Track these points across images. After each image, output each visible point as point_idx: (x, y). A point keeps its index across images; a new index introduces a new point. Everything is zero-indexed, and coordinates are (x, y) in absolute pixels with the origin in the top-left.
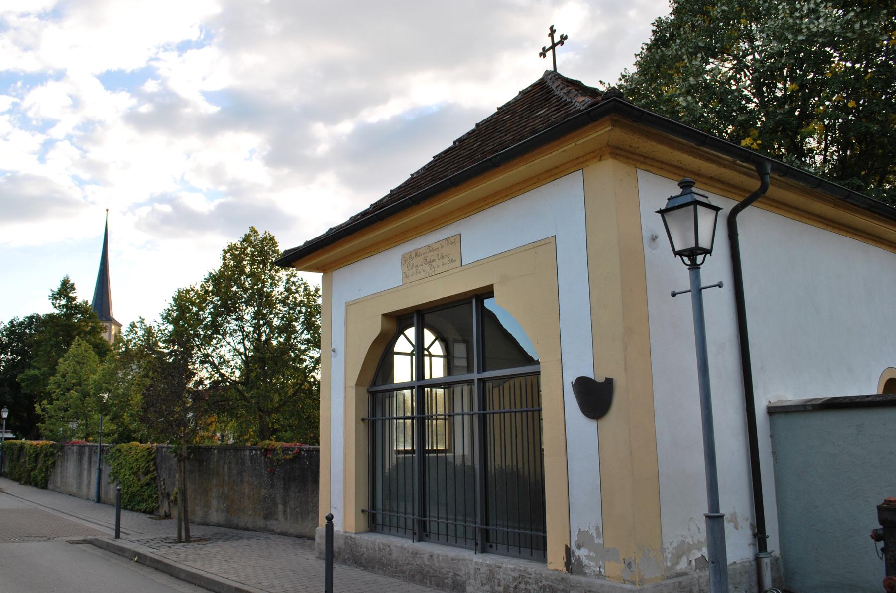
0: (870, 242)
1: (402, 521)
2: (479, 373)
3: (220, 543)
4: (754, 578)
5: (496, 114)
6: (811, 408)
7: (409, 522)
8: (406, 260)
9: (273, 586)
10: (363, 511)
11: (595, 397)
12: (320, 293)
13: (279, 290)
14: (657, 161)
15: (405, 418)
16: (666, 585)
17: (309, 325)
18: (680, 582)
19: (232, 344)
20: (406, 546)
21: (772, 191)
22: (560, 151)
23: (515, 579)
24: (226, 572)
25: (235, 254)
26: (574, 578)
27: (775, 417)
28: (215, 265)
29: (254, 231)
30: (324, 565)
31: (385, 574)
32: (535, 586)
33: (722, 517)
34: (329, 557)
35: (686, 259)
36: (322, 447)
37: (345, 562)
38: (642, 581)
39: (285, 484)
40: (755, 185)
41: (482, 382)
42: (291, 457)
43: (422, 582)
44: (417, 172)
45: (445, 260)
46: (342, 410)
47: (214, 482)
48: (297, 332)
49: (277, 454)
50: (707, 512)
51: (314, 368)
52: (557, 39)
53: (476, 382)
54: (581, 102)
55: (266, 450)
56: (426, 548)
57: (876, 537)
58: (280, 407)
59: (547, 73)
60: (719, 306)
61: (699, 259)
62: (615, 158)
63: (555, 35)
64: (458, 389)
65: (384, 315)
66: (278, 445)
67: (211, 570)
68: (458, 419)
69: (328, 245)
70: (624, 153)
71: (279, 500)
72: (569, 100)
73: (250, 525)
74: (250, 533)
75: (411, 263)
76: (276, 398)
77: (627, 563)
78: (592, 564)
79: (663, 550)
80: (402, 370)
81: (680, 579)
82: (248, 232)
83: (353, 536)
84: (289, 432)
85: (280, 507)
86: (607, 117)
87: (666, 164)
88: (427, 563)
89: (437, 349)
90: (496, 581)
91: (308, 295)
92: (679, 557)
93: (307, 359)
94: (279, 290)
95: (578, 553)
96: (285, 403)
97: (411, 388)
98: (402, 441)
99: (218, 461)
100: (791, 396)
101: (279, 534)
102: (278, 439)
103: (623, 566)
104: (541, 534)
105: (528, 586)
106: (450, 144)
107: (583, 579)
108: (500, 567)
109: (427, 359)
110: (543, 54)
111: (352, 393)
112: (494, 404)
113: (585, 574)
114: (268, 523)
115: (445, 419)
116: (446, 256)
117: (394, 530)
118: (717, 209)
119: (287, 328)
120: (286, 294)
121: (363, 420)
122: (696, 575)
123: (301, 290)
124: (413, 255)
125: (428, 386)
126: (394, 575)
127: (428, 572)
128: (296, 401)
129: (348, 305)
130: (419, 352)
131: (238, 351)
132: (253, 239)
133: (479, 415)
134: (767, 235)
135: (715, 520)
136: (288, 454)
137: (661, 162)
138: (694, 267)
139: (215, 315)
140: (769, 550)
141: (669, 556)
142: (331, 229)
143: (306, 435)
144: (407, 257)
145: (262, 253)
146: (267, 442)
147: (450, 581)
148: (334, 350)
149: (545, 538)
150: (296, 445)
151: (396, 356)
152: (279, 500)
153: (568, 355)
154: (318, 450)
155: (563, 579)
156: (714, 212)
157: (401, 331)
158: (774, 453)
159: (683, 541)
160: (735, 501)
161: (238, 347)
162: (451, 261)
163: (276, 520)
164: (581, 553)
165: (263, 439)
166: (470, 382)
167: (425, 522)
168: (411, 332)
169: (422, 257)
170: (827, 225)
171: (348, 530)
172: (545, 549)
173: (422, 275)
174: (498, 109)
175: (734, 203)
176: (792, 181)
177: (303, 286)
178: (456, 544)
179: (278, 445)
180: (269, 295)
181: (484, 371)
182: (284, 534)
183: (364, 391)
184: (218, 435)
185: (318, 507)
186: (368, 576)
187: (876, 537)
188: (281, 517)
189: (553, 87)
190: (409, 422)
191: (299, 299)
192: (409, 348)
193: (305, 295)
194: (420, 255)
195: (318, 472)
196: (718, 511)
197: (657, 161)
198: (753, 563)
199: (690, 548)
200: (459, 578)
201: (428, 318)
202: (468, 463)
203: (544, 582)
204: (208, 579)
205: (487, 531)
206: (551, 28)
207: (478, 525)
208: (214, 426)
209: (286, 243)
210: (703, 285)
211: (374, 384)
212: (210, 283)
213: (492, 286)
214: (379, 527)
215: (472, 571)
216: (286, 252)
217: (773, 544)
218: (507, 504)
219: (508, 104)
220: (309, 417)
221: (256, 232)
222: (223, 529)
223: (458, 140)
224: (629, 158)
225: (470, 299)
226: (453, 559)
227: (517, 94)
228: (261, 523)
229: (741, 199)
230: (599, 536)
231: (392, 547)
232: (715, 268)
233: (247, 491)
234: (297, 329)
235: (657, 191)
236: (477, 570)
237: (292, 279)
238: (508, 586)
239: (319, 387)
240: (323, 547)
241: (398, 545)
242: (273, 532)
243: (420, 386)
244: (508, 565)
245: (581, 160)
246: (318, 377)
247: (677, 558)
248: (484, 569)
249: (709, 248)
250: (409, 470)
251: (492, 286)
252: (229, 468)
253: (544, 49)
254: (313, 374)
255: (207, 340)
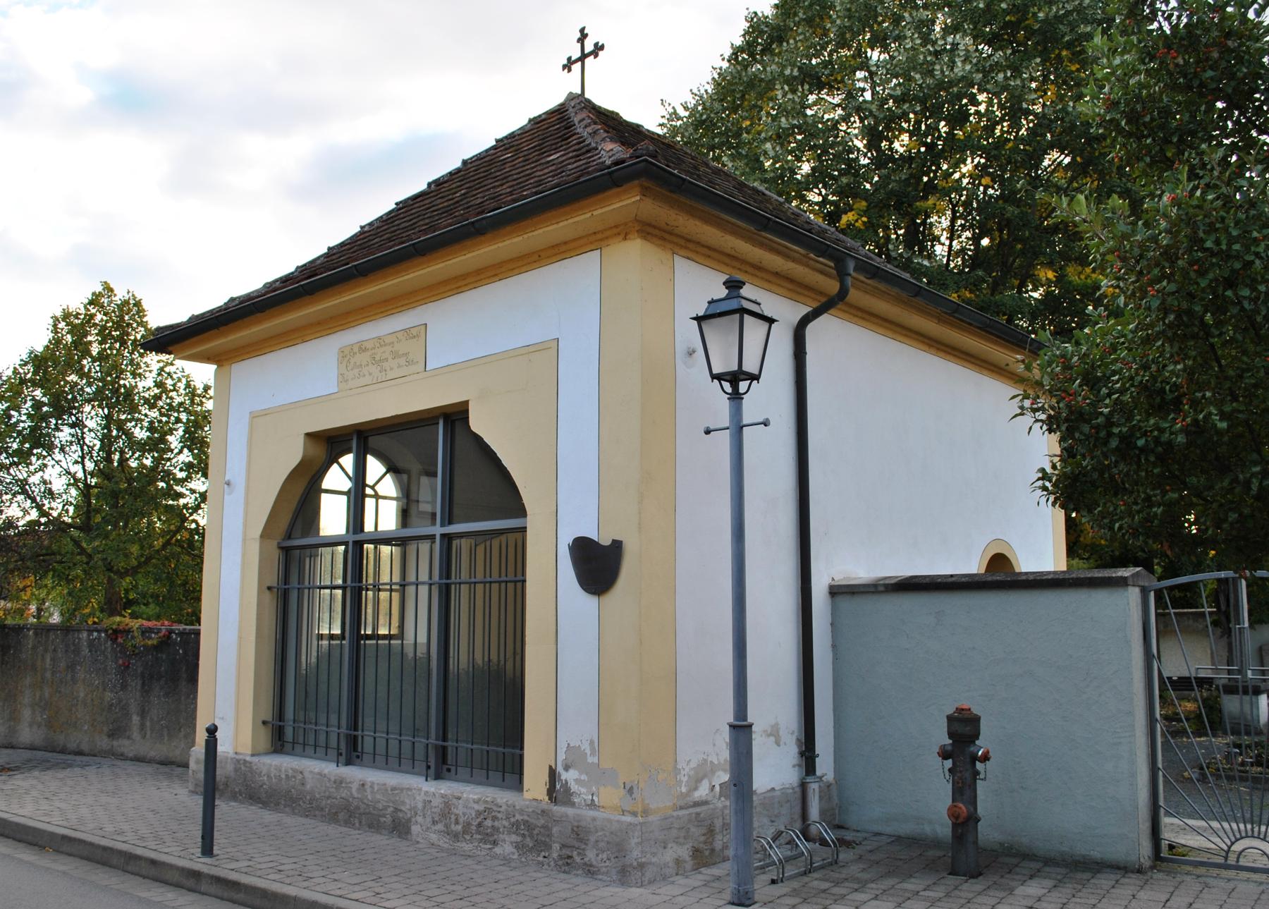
0: (986, 372)
1: (322, 738)
2: (442, 525)
3: (36, 773)
4: (798, 809)
5: (493, 148)
6: (882, 589)
7: (333, 738)
8: (345, 356)
9: (122, 833)
10: (264, 723)
11: (597, 565)
12: (211, 392)
13: (146, 385)
14: (703, 246)
15: (333, 588)
16: (678, 818)
17: (194, 441)
18: (698, 814)
19: (64, 464)
20: (326, 771)
21: (854, 295)
22: (571, 221)
23: (479, 813)
24: (46, 815)
25: (74, 329)
26: (558, 810)
27: (839, 599)
28: (40, 340)
29: (109, 289)
30: (201, 802)
31: (294, 814)
32: (506, 823)
33: (750, 726)
34: (211, 790)
35: (727, 386)
36: (205, 627)
37: (234, 797)
38: (646, 812)
39: (143, 684)
40: (833, 287)
41: (448, 538)
42: (155, 642)
43: (347, 823)
44: (370, 224)
45: (402, 361)
46: (237, 574)
47: (28, 681)
48: (172, 451)
49: (133, 637)
50: (731, 719)
51: (197, 508)
52: (589, 47)
53: (438, 538)
54: (610, 150)
55: (116, 632)
56: (355, 774)
57: (945, 754)
58: (140, 565)
59: (571, 97)
60: (770, 453)
61: (743, 386)
62: (645, 238)
63: (586, 42)
64: (412, 548)
65: (308, 435)
66: (135, 624)
67: (21, 812)
68: (411, 590)
69: (226, 324)
70: (656, 232)
71: (133, 708)
72: (593, 145)
73: (85, 747)
74: (85, 758)
75: (352, 361)
76: (135, 549)
77: (628, 787)
78: (583, 790)
79: (676, 771)
80: (333, 518)
81: (698, 810)
82: (99, 289)
83: (248, 758)
84: (152, 606)
85: (136, 719)
86: (636, 182)
87: (714, 250)
88: (356, 795)
89: (388, 487)
90: (453, 817)
91: (192, 393)
92: (699, 781)
93: (188, 493)
94: (146, 385)
95: (565, 776)
96: (149, 559)
97: (346, 544)
98: (328, 622)
99: (34, 648)
100: (863, 572)
101: (131, 760)
102: (134, 616)
103: (622, 792)
104: (518, 751)
105: (496, 824)
106: (423, 187)
107: (570, 811)
108: (459, 798)
109: (370, 504)
110: (568, 66)
111: (255, 548)
112: (462, 571)
113: (573, 804)
114: (115, 743)
115: (391, 590)
116: (406, 354)
117: (310, 750)
118: (771, 321)
119: (157, 443)
120: (157, 391)
121: (269, 588)
122: (720, 805)
123: (182, 385)
124: (356, 349)
125: (370, 542)
126: (307, 814)
127: (358, 808)
128: (167, 558)
129: (254, 416)
130: (358, 495)
131: (74, 476)
132: (105, 300)
133: (440, 585)
134: (848, 353)
135: (741, 730)
136: (150, 638)
137: (709, 248)
138: (736, 396)
139: (38, 415)
140: (818, 773)
141: (685, 779)
142: (232, 300)
143: (181, 609)
144: (347, 352)
145: (119, 325)
146: (118, 619)
147: (388, 819)
148: (228, 484)
149: (521, 757)
150: (164, 625)
151: (323, 496)
152: (133, 708)
153: (564, 507)
154: (198, 633)
155: (543, 811)
156: (766, 325)
157: (333, 459)
158: (834, 646)
159: (705, 760)
160: (774, 706)
161: (73, 469)
162: (409, 363)
163: (129, 738)
164: (570, 776)
165: (113, 613)
166: (431, 538)
167: (355, 737)
168: (348, 460)
169: (369, 353)
170: (930, 346)
171: (240, 750)
172: (521, 774)
173: (367, 380)
174: (497, 141)
175: (805, 310)
176: (882, 286)
177: (184, 381)
178: (399, 768)
179: (135, 624)
180: (130, 393)
181: (450, 523)
182: (138, 759)
183: (273, 545)
184: (33, 608)
185: (195, 719)
186: (269, 816)
187: (945, 754)
188: (136, 735)
189: (576, 120)
190: (339, 592)
191: (178, 400)
192: (346, 485)
193: (186, 395)
194: (366, 350)
195: (197, 666)
196: (745, 719)
197: (703, 246)
198: (798, 790)
199: (714, 769)
200: (401, 815)
201: (373, 441)
202: (421, 651)
203: (518, 817)
204: (17, 824)
205: (444, 749)
206: (582, 30)
207: (432, 741)
208: (29, 593)
209: (161, 315)
210: (745, 422)
211: (289, 536)
212: (29, 366)
213: (467, 402)
214: (288, 747)
215: (420, 805)
216: (159, 329)
217: (825, 765)
218: (478, 716)
219: (512, 136)
220: (185, 584)
221: (112, 290)
222: (39, 754)
223: (434, 182)
224: (664, 239)
225: (437, 418)
226: (393, 789)
227: (525, 122)
228: (103, 742)
229: (815, 305)
230: (592, 754)
231: (306, 774)
232: (769, 398)
233: (82, 695)
234: (173, 447)
235: (700, 285)
236: (427, 803)
237: (167, 369)
238: (469, 824)
239: (203, 537)
240: (201, 776)
241: (316, 770)
242: (122, 757)
243: (357, 541)
244: (469, 795)
245: (599, 236)
246: (202, 522)
247: (696, 782)
248: (437, 802)
249: (756, 372)
250: (335, 667)
251: (467, 402)
252: (53, 659)
253: (569, 59)
254: (195, 517)
255: (23, 457)
